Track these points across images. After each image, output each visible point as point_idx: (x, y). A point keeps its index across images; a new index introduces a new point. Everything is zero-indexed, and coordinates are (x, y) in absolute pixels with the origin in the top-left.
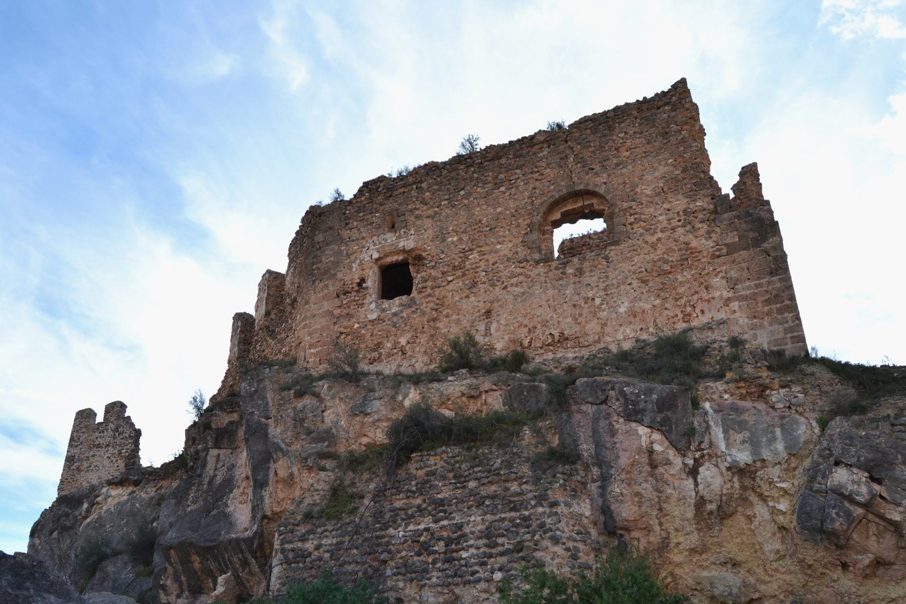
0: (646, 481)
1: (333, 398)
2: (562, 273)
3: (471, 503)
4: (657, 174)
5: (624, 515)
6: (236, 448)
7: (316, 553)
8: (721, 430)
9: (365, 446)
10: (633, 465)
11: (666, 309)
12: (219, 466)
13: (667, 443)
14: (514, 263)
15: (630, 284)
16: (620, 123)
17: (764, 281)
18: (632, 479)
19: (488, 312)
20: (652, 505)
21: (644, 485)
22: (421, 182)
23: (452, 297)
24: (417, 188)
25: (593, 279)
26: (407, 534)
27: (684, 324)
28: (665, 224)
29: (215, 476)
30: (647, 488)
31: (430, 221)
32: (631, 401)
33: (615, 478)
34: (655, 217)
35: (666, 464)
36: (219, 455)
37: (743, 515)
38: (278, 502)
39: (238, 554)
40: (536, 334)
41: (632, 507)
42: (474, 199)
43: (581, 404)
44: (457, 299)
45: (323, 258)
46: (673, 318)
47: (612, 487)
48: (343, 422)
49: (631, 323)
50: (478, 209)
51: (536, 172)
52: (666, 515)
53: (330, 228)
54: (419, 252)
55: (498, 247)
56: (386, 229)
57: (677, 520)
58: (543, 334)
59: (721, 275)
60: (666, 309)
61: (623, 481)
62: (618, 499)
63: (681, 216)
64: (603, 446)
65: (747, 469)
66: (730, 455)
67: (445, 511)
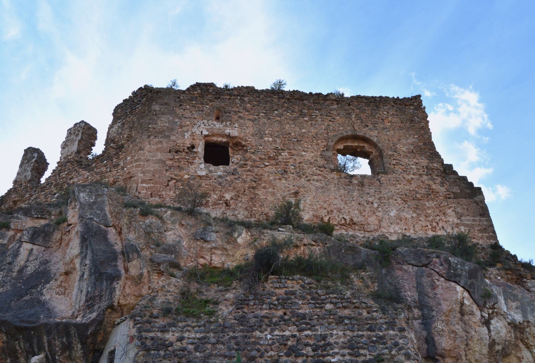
0: (458, 324)
1: (173, 223)
2: (349, 182)
3: (331, 320)
4: (409, 141)
5: (443, 345)
6: (49, 247)
7: (179, 344)
8: (503, 298)
9: (201, 265)
10: (450, 311)
11: (420, 220)
12: (31, 259)
13: (471, 300)
14: (315, 166)
15: (396, 200)
16: (383, 106)
17: (477, 218)
18: (449, 321)
19: (296, 193)
20: (462, 341)
21: (457, 326)
22: (244, 96)
23: (268, 176)
24: (240, 99)
25: (372, 190)
26: (275, 337)
27: (432, 232)
28: (415, 171)
29: (27, 267)
30: (458, 328)
31: (251, 123)
32: (453, 267)
33: (438, 318)
34: (409, 165)
35: (470, 314)
36: (32, 250)
37: (515, 356)
38: (124, 296)
39: (62, 338)
40: (333, 216)
41: (449, 340)
42: (285, 119)
43: (404, 264)
44: (272, 178)
45: (159, 122)
46: (425, 227)
47: (436, 324)
48: (184, 243)
49: (398, 224)
50: (288, 126)
51: (329, 116)
52: (470, 349)
53: (166, 104)
54: (240, 141)
55: (304, 153)
56: (214, 118)
57: (477, 354)
58: (338, 217)
59: (451, 209)
60: (420, 220)
61: (443, 321)
62: (440, 333)
63: (424, 169)
64: (426, 295)
65: (519, 326)
66: (510, 315)
67: (307, 324)
